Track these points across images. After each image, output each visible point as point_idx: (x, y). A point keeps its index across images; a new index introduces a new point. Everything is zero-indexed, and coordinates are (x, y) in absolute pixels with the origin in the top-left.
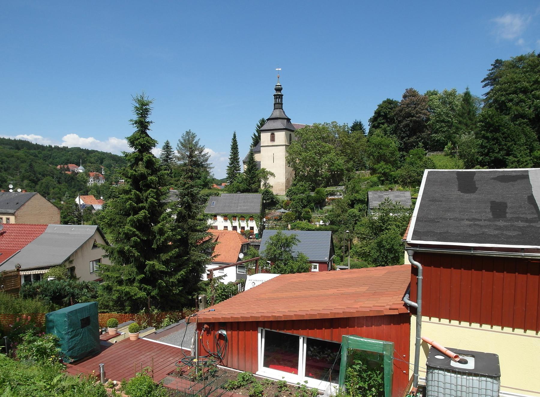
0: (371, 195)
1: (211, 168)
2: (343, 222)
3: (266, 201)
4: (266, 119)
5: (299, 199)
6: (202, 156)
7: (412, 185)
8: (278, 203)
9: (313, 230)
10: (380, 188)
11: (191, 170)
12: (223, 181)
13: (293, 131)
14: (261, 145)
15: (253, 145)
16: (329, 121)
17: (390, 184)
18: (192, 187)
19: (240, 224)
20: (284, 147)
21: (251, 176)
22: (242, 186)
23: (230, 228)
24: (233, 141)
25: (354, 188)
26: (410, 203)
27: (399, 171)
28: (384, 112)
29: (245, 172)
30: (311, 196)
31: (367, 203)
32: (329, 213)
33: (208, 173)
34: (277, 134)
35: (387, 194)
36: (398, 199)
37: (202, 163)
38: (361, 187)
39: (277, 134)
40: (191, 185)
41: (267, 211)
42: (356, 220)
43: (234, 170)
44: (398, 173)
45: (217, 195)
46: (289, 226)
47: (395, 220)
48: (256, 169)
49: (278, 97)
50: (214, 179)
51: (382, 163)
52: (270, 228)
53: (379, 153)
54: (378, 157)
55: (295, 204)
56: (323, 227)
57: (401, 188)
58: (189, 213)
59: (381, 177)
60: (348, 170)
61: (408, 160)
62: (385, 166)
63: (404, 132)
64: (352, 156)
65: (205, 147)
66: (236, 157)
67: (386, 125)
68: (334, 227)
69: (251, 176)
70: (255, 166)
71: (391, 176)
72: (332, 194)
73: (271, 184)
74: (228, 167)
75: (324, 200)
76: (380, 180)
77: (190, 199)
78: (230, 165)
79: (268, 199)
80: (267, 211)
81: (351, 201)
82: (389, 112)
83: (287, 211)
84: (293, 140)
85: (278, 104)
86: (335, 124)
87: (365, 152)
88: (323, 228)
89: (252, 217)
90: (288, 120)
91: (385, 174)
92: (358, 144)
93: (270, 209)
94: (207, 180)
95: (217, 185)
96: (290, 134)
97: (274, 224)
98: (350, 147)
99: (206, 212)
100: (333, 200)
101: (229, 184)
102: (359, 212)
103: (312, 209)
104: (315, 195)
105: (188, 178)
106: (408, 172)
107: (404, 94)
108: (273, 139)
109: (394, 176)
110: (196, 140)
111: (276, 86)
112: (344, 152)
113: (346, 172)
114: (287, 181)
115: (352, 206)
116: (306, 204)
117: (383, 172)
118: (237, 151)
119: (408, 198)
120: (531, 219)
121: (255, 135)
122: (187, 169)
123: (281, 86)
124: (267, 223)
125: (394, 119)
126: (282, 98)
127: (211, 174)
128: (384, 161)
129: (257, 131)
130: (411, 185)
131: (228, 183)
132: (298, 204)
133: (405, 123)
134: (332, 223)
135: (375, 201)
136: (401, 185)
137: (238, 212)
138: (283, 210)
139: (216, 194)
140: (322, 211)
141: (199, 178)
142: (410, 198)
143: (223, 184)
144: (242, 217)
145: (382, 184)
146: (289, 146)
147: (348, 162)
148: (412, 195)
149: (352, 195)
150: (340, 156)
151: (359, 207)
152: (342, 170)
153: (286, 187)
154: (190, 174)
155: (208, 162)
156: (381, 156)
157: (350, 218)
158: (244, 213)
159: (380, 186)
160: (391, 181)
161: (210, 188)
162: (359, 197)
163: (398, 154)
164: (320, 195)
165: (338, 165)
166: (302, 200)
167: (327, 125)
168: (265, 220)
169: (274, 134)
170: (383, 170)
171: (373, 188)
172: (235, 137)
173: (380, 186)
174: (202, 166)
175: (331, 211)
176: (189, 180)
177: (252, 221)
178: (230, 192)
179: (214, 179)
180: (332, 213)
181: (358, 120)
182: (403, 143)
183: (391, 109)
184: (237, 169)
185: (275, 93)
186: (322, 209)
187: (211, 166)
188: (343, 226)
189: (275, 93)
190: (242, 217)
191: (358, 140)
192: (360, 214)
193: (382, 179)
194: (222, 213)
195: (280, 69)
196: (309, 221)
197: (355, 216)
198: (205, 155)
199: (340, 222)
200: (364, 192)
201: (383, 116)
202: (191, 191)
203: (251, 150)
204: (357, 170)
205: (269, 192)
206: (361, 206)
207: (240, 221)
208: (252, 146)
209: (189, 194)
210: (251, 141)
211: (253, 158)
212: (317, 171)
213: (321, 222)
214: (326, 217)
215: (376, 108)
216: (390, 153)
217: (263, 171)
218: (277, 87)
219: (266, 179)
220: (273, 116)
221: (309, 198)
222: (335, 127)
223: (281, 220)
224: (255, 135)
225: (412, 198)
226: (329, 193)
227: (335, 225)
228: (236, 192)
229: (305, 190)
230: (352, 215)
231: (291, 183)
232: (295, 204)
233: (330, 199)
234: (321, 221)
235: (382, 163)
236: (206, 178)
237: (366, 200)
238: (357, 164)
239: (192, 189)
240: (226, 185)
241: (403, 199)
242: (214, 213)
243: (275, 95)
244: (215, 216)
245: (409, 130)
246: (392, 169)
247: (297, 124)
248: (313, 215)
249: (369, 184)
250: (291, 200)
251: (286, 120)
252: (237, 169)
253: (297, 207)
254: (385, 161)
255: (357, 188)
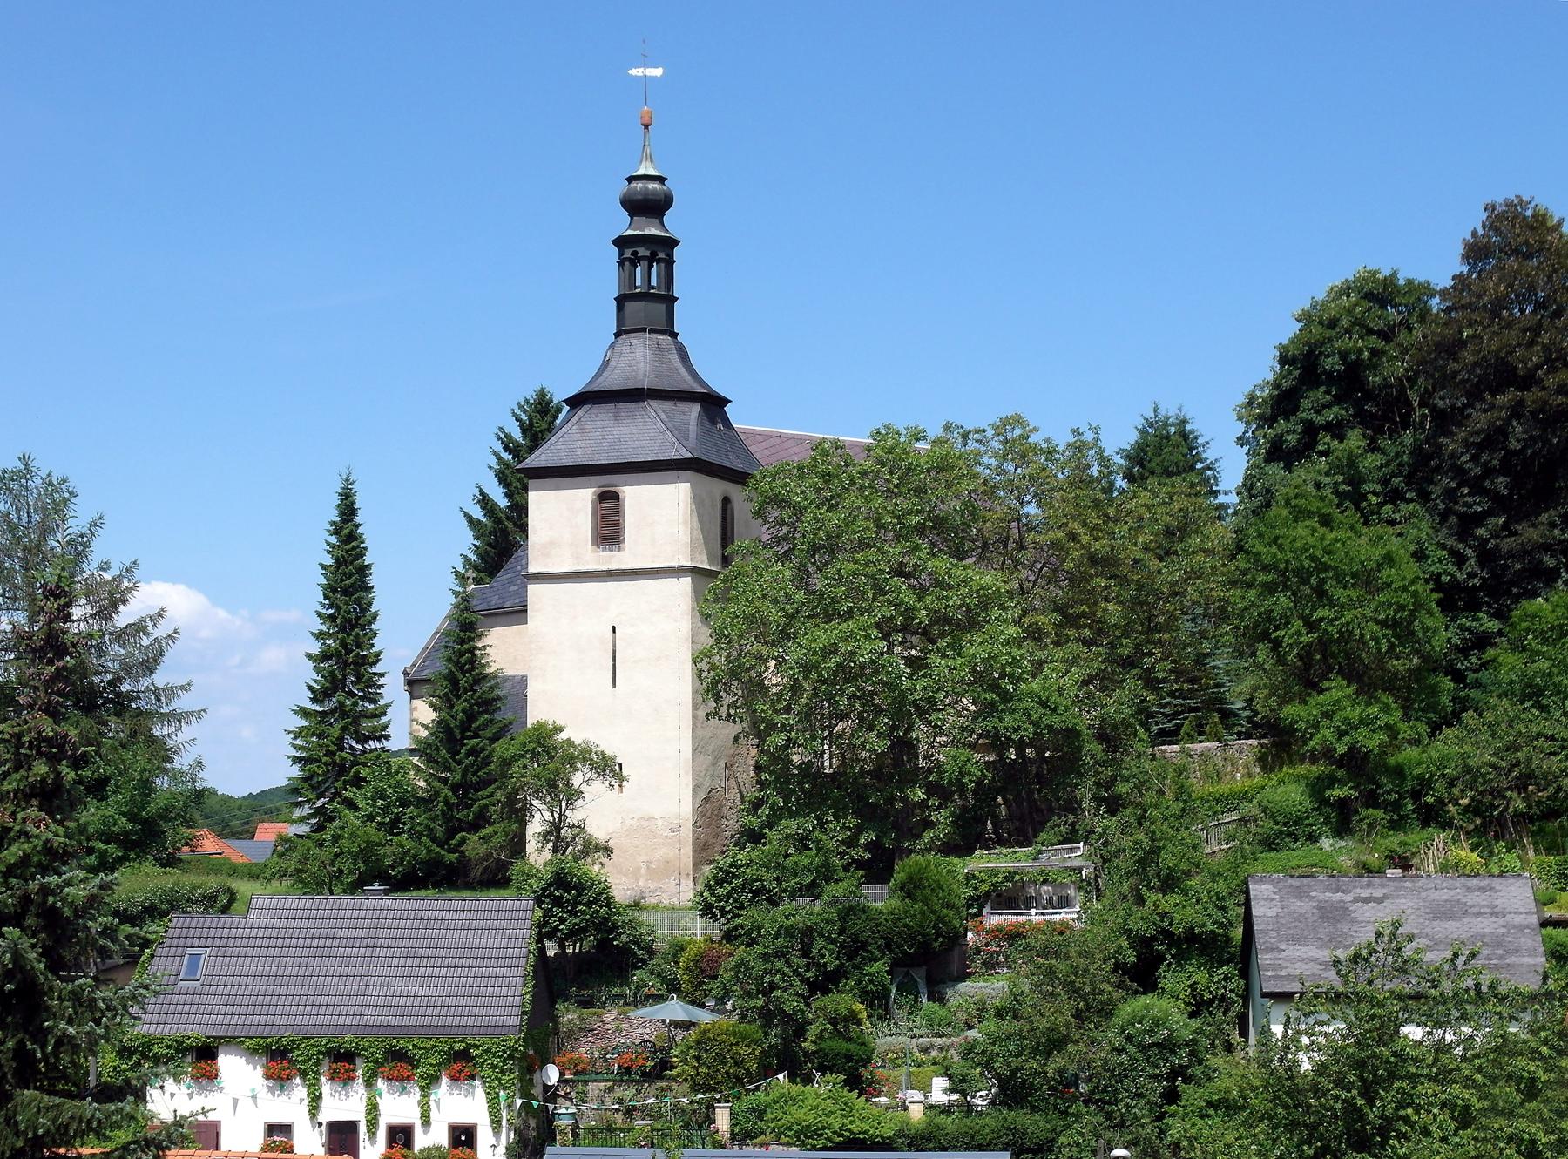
0: (1267, 900)
1: (179, 718)
2: (1084, 1088)
3: (562, 946)
4: (560, 393)
5: (789, 932)
6: (120, 636)
7: (1541, 830)
8: (644, 962)
9: (885, 1145)
10: (1328, 855)
11: (47, 740)
12: (261, 806)
13: (740, 478)
14: (533, 569)
15: (476, 568)
16: (979, 415)
17: (1395, 826)
18: (54, 858)
19: (373, 1110)
20: (686, 581)
21: (458, 777)
22: (396, 847)
23: (309, 1142)
24: (334, 540)
25: (1147, 859)
26: (1531, 952)
27: (1448, 743)
28: (1344, 355)
29: (422, 749)
30: (865, 910)
31: (1244, 957)
32: (992, 1026)
33: (161, 753)
34: (637, 497)
35: (1378, 893)
36: (1453, 929)
37: (115, 682)
38: (1195, 847)
39: (637, 497)
40: (48, 849)
41: (568, 1016)
42: (1175, 1073)
43: (341, 739)
44: (1445, 758)
45: (222, 903)
46: (723, 1119)
47: (1444, 1077)
48: (494, 729)
49: (643, 252)
50: (200, 796)
51: (1338, 690)
52: (590, 1130)
53: (1311, 626)
54: (1306, 656)
55: (758, 967)
56: (949, 1123)
57: (1465, 853)
58: (21, 1044)
59: (1332, 781)
60: (1110, 737)
61: (1509, 665)
62: (1354, 713)
63: (1477, 488)
64: (1138, 647)
65: (137, 574)
66: (359, 646)
67: (1355, 440)
68: (1021, 1118)
69: (458, 777)
70: (489, 704)
71: (1399, 772)
72: (1010, 896)
73: (598, 829)
74: (304, 713)
75: (955, 939)
76: (1323, 802)
77: (33, 946)
78: (314, 700)
79: (576, 934)
80: (568, 1016)
81: (1132, 947)
82: (1375, 353)
83: (704, 1017)
84: (742, 542)
85: (645, 296)
86: (1018, 432)
87: (1223, 615)
88: (950, 1128)
89: (463, 1056)
90: (713, 405)
91: (1355, 763)
92: (1173, 572)
93: (586, 1003)
94: (154, 806)
95: (225, 831)
96: (726, 501)
97: (620, 1101)
98: (1124, 581)
99: (148, 1025)
100: (1013, 936)
101: (304, 829)
102: (1192, 1015)
103: (878, 1001)
104: (895, 903)
105: (27, 798)
106: (1513, 747)
107: (1474, 233)
108: (608, 529)
109: (1420, 778)
110: (77, 523)
111: (631, 179)
112: (1082, 615)
113: (1093, 748)
114: (708, 809)
115: (1143, 975)
116: (831, 962)
117: (1341, 748)
118: (365, 607)
119: (1518, 919)
120: (132, 855)
121: (485, 501)
122: (19, 736)
123: (661, 180)
124: (567, 1097)
125: (1408, 403)
126: (669, 262)
127: (182, 762)
128: (1349, 675)
129: (502, 478)
130: (1533, 834)
131: (302, 820)
132: (779, 964)
133: (1480, 419)
134: (1013, 1093)
135: (1298, 940)
136: (1468, 834)
137: (371, 1020)
138: (676, 1009)
139: (209, 900)
140: (942, 1012)
141: (98, 788)
142: (1534, 920)
143: (268, 832)
144: (397, 1055)
145: (1342, 829)
146: (711, 574)
147: (1105, 681)
148: (1543, 903)
149: (1141, 901)
150: (1057, 644)
151: (1193, 986)
152: (1071, 734)
153: (702, 850)
154: (41, 768)
155: (161, 678)
156: (1324, 644)
157: (1131, 1058)
158: (408, 1032)
159: (1326, 843)
160: (1396, 806)
161: (171, 862)
162: (1188, 913)
163: (1442, 634)
164: (926, 901)
165: (1044, 704)
166: (807, 934)
167: (965, 437)
168: (552, 1074)
169: (615, 497)
170: (1341, 734)
171: (1283, 854)
172: (348, 509)
173: (1326, 843)
174: (121, 704)
175: (1000, 1014)
176: (33, 812)
177: (464, 1086)
178: (314, 882)
179: (202, 791)
180: (1010, 1026)
181: (1169, 409)
182: (1469, 552)
183: (1387, 335)
184: (366, 725)
185: (623, 225)
186: (942, 1000)
187: (182, 703)
188: (1091, 1117)
189: (623, 225)
190: (397, 1055)
191: (1171, 539)
192: (1199, 1031)
193: (1338, 792)
194: (253, 1031)
195: (657, 72)
196: (855, 1082)
197: (1168, 1046)
198: (139, 628)
199: (1067, 1086)
200: (1220, 886)
201: (1330, 378)
202: (45, 891)
203: (464, 604)
204: (1168, 736)
205: (581, 887)
206: (1201, 977)
207: (381, 1084)
208: (471, 574)
209: (33, 909)
210: (464, 543)
211: (472, 650)
212: (904, 747)
213: (939, 1090)
214: (968, 1051)
215: (1287, 330)
216: (1383, 624)
217: (544, 742)
218: (639, 185)
219: (560, 791)
220: (612, 381)
221: (857, 924)
222: (1019, 450)
223: (661, 1077)
224: (485, 501)
225: (1544, 924)
226: (984, 887)
227: (1034, 1109)
228: (357, 886)
229: (827, 873)
230: (1148, 1040)
231: (732, 824)
232: (758, 967)
233: (995, 932)
234: (940, 1083)
235: (1338, 690)
236: (146, 787)
237: (1237, 933)
238: (1172, 694)
239: (52, 879)
240: (284, 840)
241: (1486, 926)
242: (195, 1029)
243: (621, 242)
244: (206, 1053)
245: (1505, 469)
246: (1403, 726)
247: (769, 436)
248: (885, 1040)
249: (1252, 827)
250: (729, 937)
251: (695, 409)
252: (366, 725)
253: (773, 986)
254: (1352, 673)
255: (1167, 859)
